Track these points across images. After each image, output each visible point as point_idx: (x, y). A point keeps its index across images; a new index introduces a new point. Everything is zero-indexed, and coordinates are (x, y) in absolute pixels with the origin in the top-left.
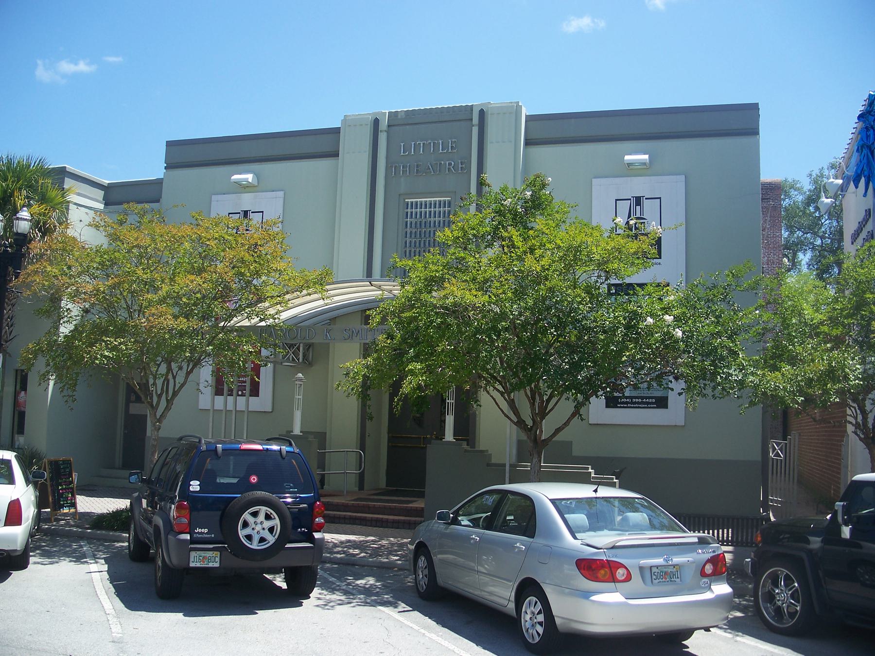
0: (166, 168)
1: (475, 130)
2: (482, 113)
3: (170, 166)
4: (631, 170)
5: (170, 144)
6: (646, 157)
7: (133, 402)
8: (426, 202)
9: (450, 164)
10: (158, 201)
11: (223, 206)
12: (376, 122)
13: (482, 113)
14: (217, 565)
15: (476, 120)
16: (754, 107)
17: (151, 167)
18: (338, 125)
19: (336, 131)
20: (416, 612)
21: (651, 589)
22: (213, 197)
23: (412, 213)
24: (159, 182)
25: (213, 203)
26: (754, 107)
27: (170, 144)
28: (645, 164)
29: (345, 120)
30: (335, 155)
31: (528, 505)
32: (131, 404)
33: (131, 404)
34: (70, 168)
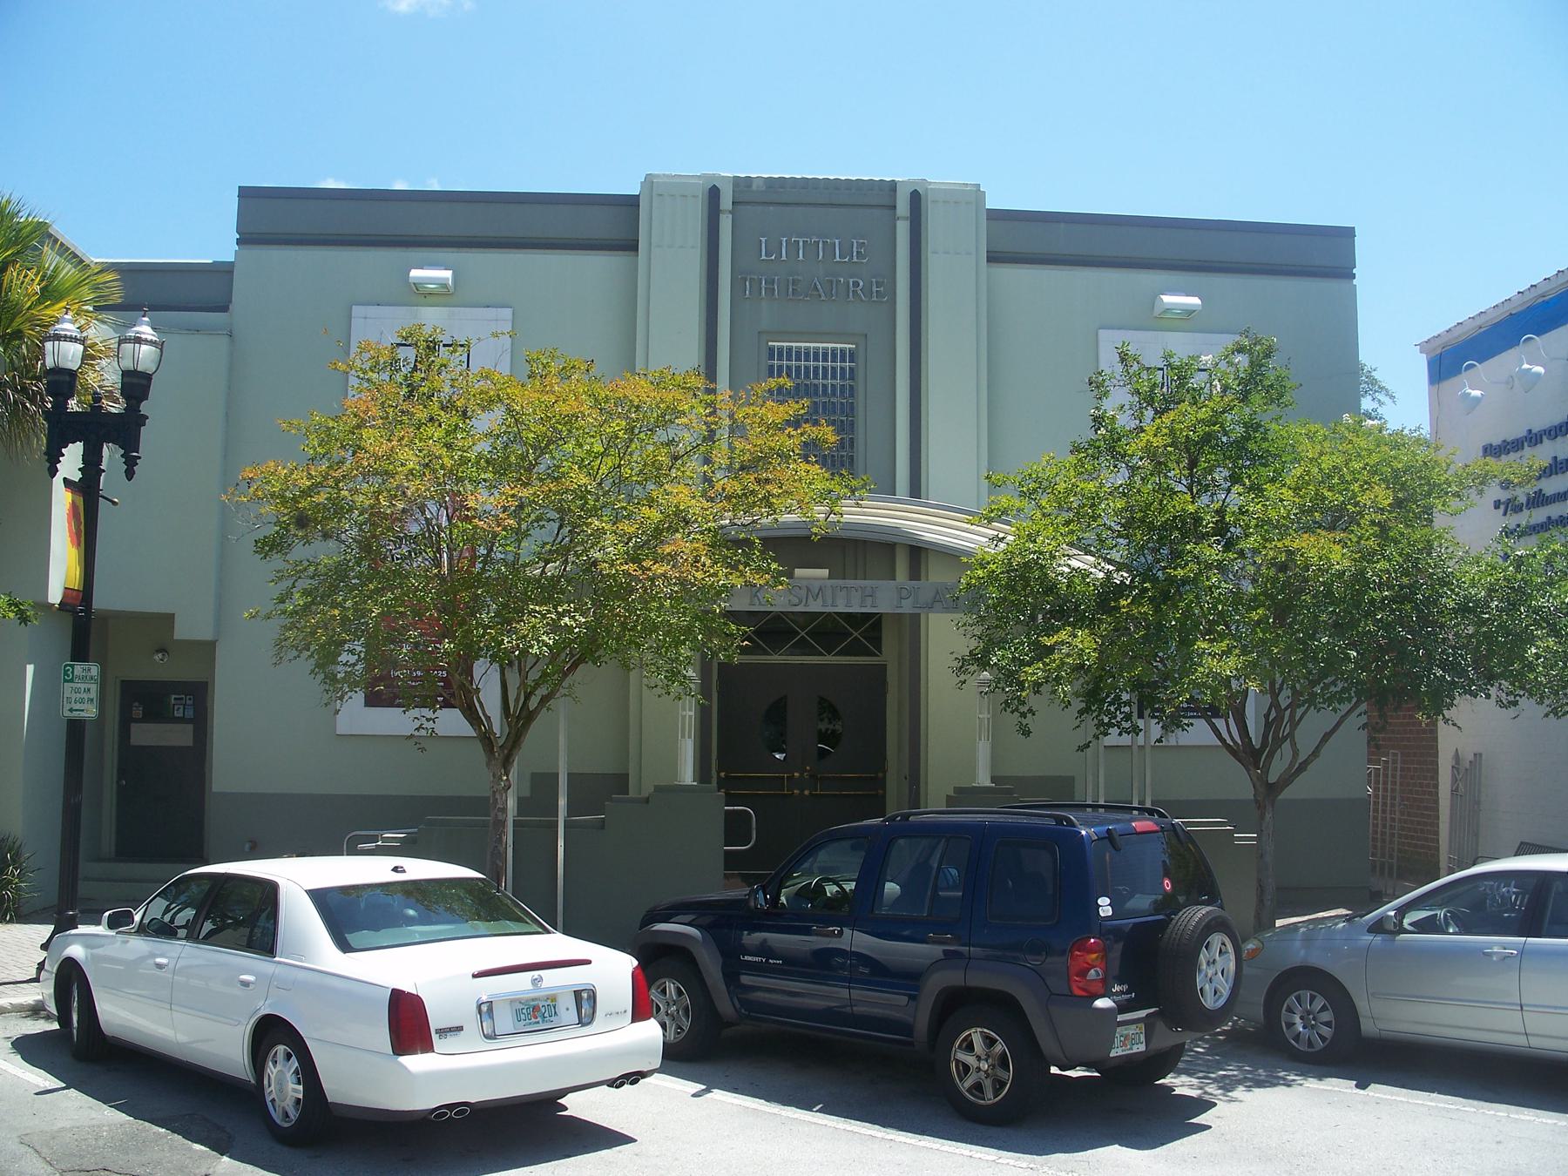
0: (239, 242)
1: (903, 229)
2: (916, 198)
3: (247, 238)
4: (422, 295)
5: (245, 194)
6: (448, 274)
7: (137, 721)
8: (807, 349)
9: (856, 284)
10: (225, 309)
11: (378, 328)
12: (714, 193)
13: (916, 198)
14: (1142, 1048)
15: (903, 207)
16: (1349, 233)
17: (212, 241)
18: (634, 190)
19: (632, 202)
20: (73, 1092)
21: (521, 1027)
22: (357, 311)
23: (798, 368)
24: (222, 273)
25: (1101, 344)
26: (1349, 233)
27: (245, 194)
28: (445, 286)
29: (649, 181)
30: (631, 246)
31: (268, 892)
32: (134, 727)
33: (134, 727)
34: (57, 229)
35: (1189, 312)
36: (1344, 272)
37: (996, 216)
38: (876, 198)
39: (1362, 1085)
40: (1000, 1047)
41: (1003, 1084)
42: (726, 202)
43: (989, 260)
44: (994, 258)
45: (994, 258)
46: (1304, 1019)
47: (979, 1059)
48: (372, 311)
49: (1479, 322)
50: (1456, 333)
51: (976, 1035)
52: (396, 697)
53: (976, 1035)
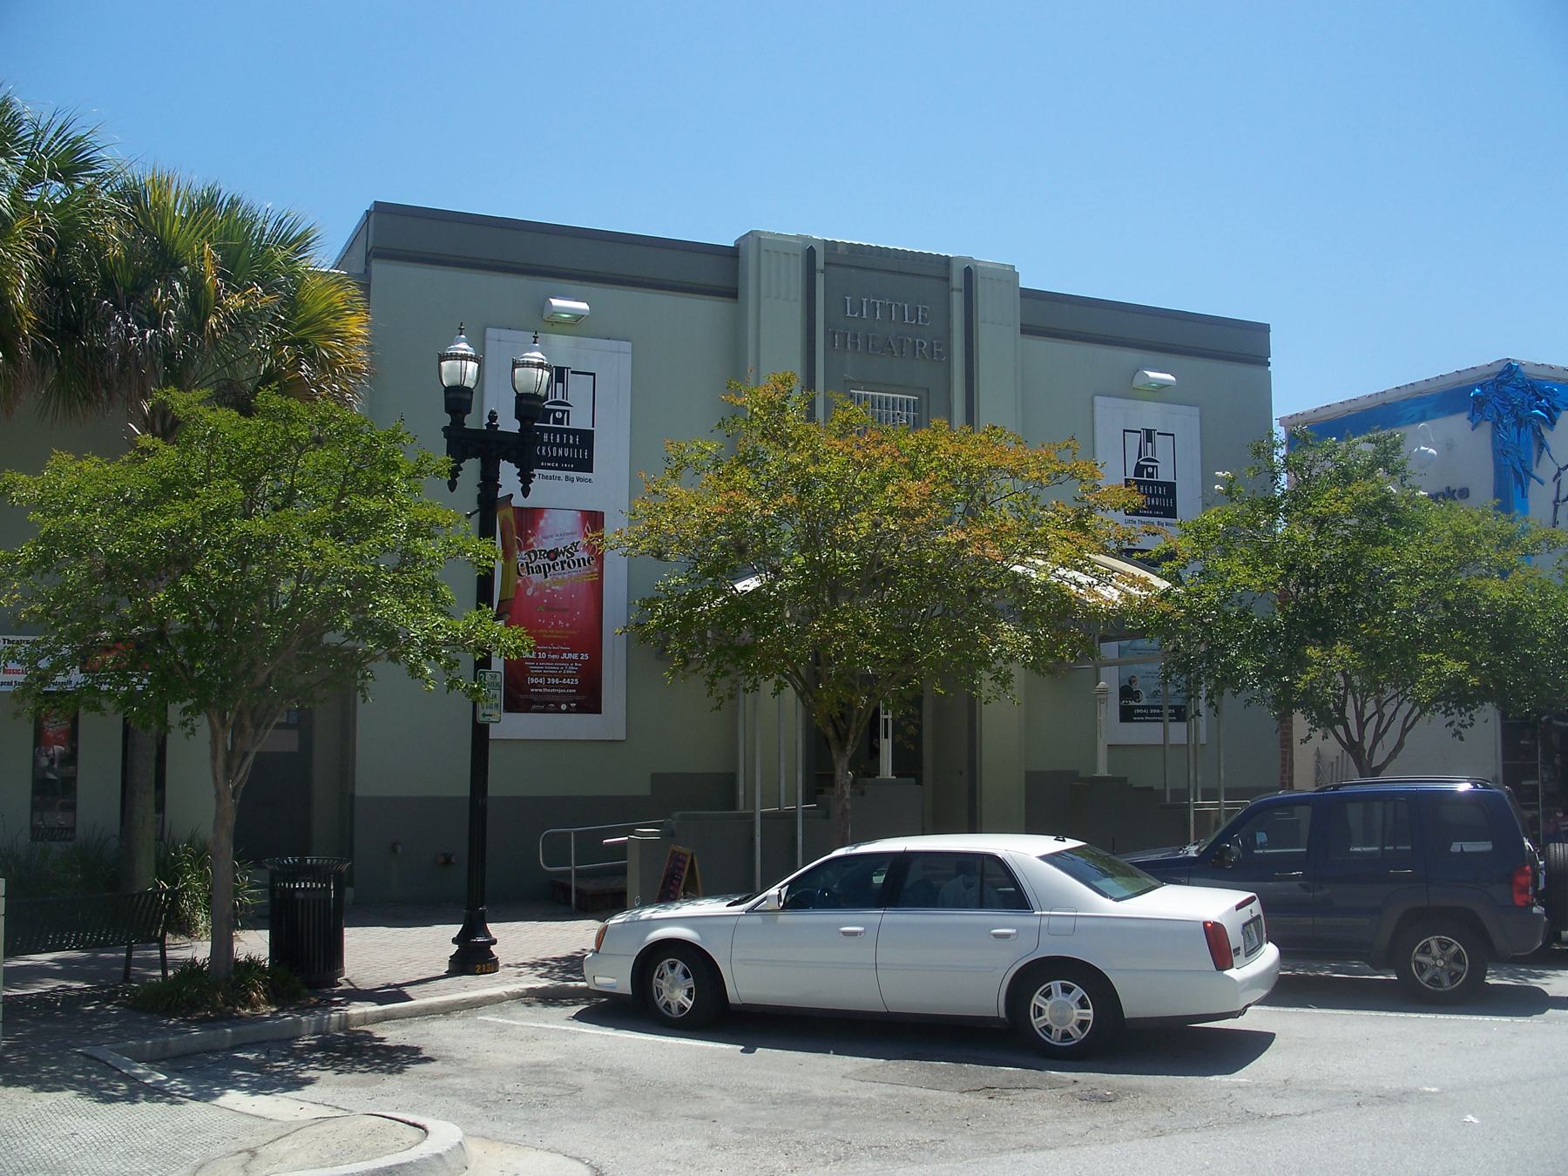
1: (957, 300)
12: (810, 253)
15: (957, 280)
16: (1265, 329)
22: (1196, 410)
25: (488, 343)
26: (1265, 329)
30: (731, 293)
35: (578, 317)
36: (1261, 359)
37: (1027, 294)
38: (932, 274)
39: (749, 1049)
40: (1456, 946)
41: (1458, 974)
42: (820, 264)
43: (1023, 332)
44: (1026, 330)
45: (1026, 330)
46: (677, 992)
47: (1435, 958)
48: (504, 333)
49: (1349, 407)
50: (1323, 413)
51: (1433, 942)
52: (532, 702)
53: (1433, 942)
